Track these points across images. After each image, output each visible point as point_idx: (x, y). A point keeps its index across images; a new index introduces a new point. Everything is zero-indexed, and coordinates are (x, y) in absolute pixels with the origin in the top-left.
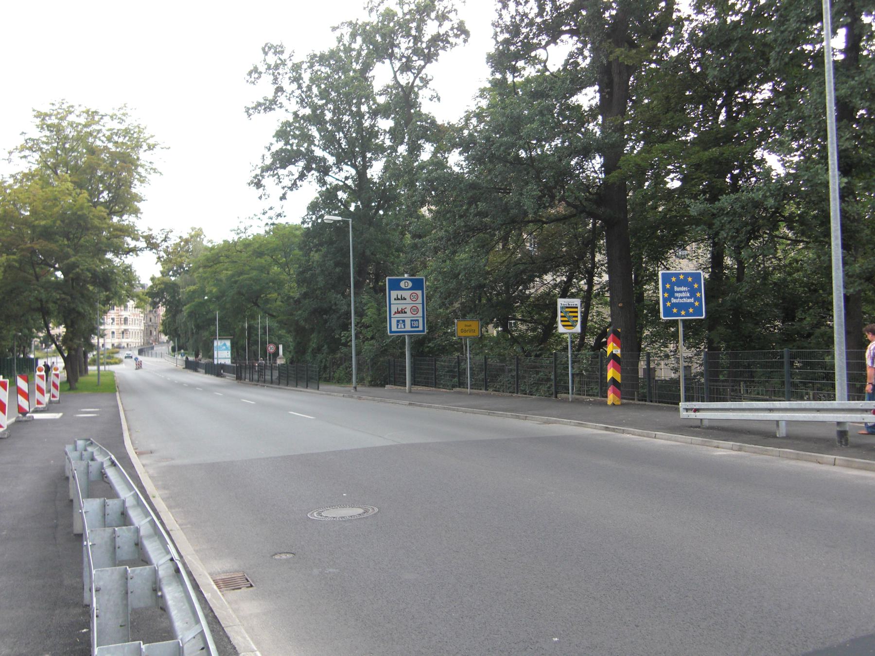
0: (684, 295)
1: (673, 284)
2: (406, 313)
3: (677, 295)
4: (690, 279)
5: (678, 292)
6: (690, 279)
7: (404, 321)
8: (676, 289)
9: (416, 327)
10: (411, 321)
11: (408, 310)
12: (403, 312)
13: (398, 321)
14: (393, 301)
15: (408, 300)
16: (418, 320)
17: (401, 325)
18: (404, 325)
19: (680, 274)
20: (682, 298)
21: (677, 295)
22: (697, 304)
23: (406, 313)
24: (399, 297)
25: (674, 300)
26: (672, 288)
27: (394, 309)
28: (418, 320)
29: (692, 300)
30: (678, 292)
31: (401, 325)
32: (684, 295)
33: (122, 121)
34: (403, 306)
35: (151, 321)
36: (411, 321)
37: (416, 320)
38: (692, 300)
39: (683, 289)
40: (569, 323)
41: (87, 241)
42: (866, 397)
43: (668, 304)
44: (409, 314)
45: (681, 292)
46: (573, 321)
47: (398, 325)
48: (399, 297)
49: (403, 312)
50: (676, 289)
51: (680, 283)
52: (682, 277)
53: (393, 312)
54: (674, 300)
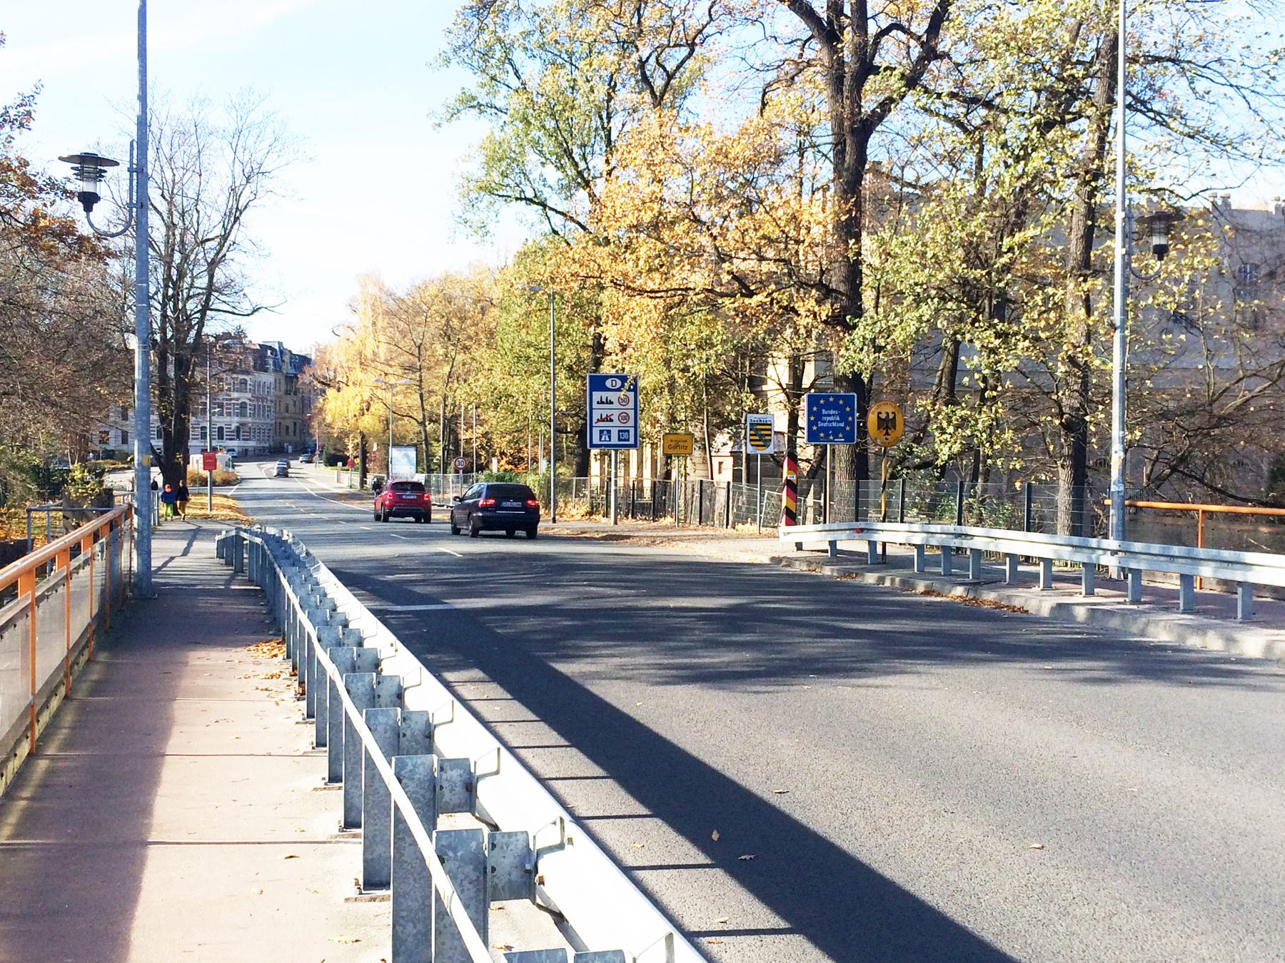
0: (831, 418)
1: (820, 407)
2: (612, 421)
3: (824, 418)
4: (841, 402)
5: (825, 415)
6: (841, 402)
7: (609, 432)
8: (824, 412)
9: (625, 440)
10: (619, 431)
11: (615, 418)
12: (609, 419)
13: (601, 432)
14: (595, 405)
15: (616, 405)
16: (628, 431)
17: (605, 437)
18: (610, 437)
19: (830, 396)
20: (830, 422)
21: (824, 418)
22: (848, 428)
23: (612, 421)
24: (604, 400)
25: (820, 424)
26: (819, 411)
27: (596, 416)
28: (628, 431)
29: (842, 425)
30: (825, 415)
31: (605, 437)
32: (831, 418)
33: (367, 327)
34: (609, 412)
35: (287, 411)
36: (619, 431)
37: (625, 431)
38: (842, 425)
39: (832, 412)
40: (761, 443)
41: (75, 587)
42: (124, 447)
43: (815, 428)
44: (616, 422)
45: (829, 415)
46: (766, 441)
47: (601, 437)
48: (604, 400)
49: (609, 419)
50: (824, 412)
51: (828, 406)
52: (831, 399)
53: (595, 420)
54: (820, 424)
